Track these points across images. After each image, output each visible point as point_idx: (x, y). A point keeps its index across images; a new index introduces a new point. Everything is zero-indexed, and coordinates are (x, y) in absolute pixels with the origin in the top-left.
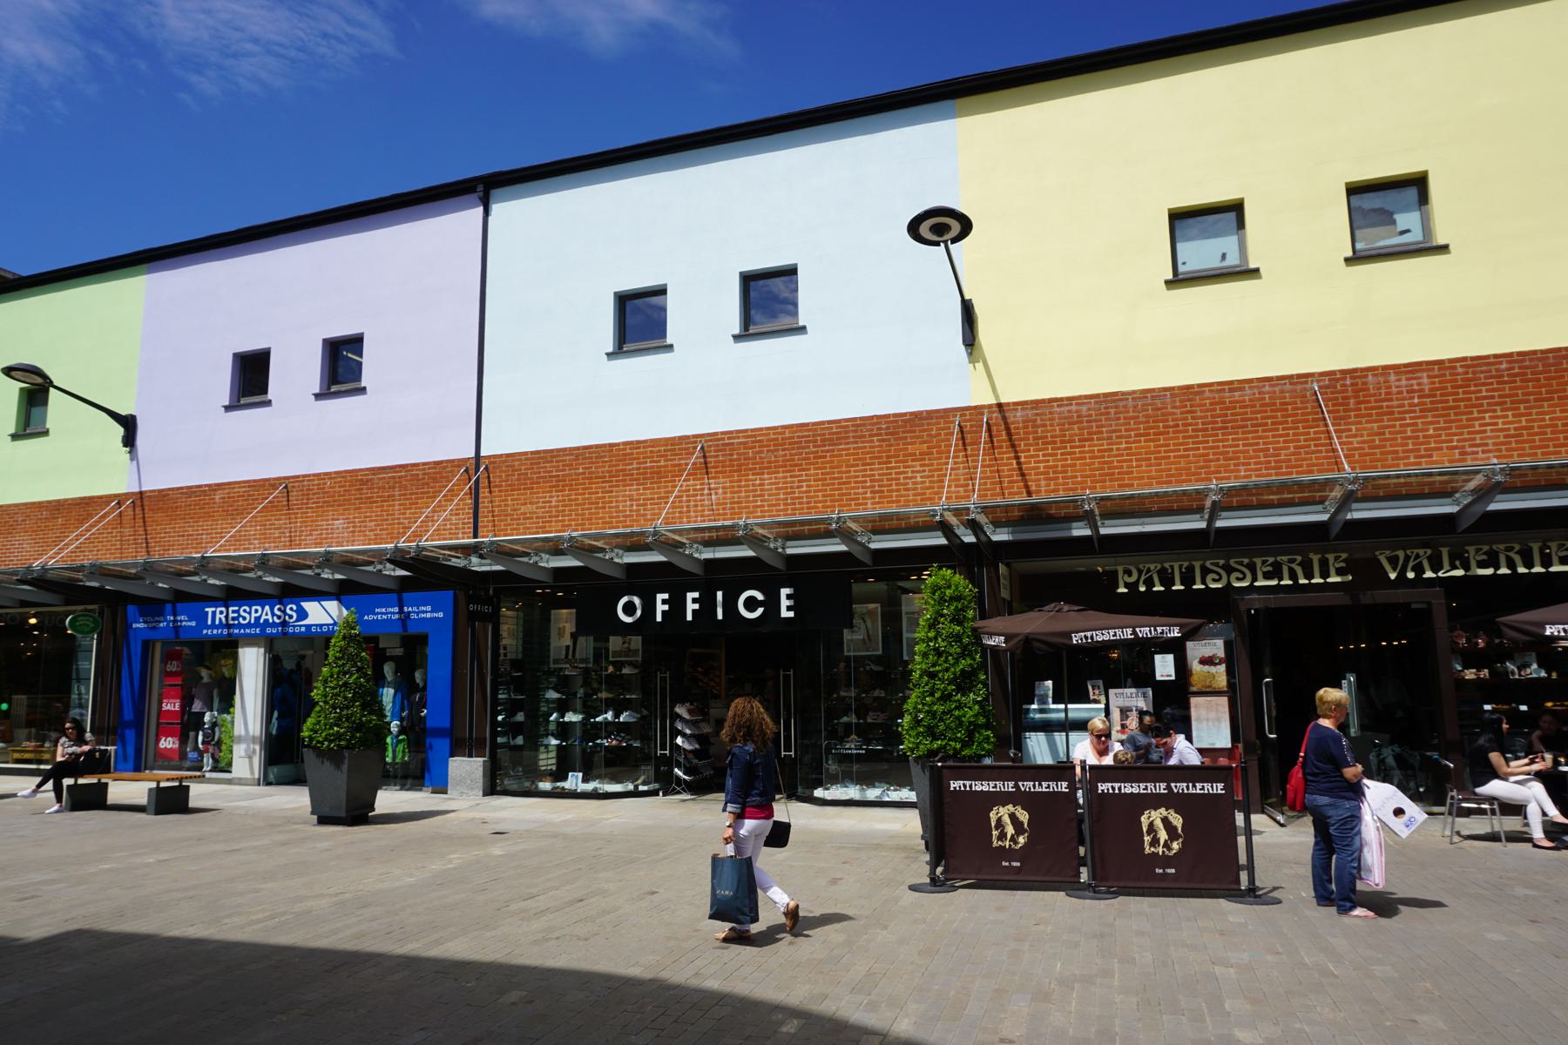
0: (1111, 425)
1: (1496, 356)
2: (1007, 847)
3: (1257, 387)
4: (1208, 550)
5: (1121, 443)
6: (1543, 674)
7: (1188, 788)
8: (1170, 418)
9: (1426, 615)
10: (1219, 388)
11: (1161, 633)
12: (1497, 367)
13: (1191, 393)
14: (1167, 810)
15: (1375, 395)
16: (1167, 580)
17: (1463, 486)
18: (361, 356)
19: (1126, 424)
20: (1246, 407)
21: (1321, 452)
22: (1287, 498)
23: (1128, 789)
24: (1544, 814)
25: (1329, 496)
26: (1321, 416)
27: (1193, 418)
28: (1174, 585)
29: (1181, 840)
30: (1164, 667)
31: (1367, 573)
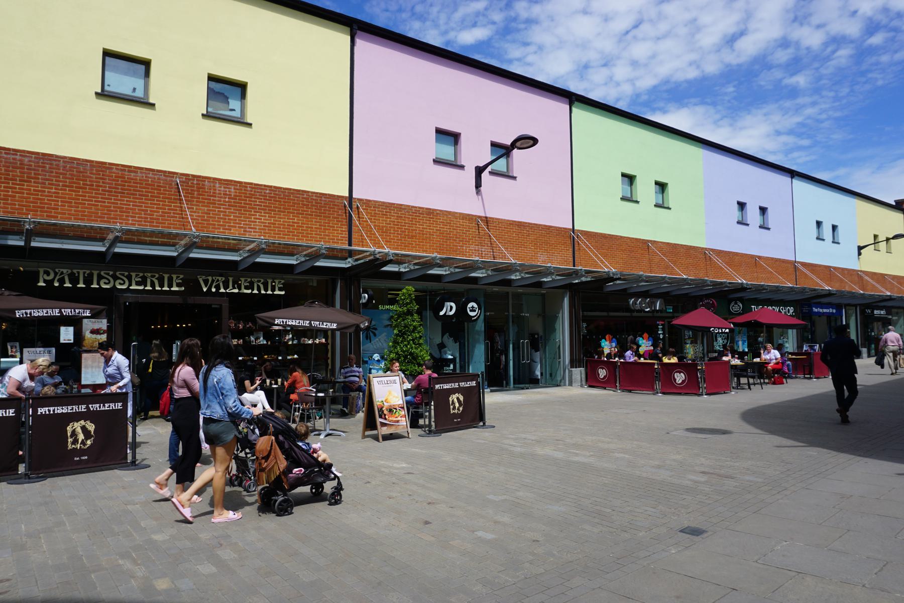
0: (46, 175)
1: (265, 186)
2: (78, 448)
3: (145, 173)
4: (104, 265)
5: (52, 188)
6: (265, 342)
7: (100, 407)
8: (88, 179)
9: (218, 312)
10: (122, 168)
11: (78, 313)
12: (265, 191)
13: (104, 167)
14: (85, 422)
15: (208, 192)
16: (74, 280)
17: (244, 248)
18: (622, 187)
19: (57, 177)
20: (137, 183)
21: (176, 217)
22: (154, 240)
23: (60, 410)
24: (264, 408)
25: (179, 243)
26: (178, 197)
27: (103, 183)
28: (92, 284)
29: (92, 439)
30: (67, 334)
31: (192, 286)
